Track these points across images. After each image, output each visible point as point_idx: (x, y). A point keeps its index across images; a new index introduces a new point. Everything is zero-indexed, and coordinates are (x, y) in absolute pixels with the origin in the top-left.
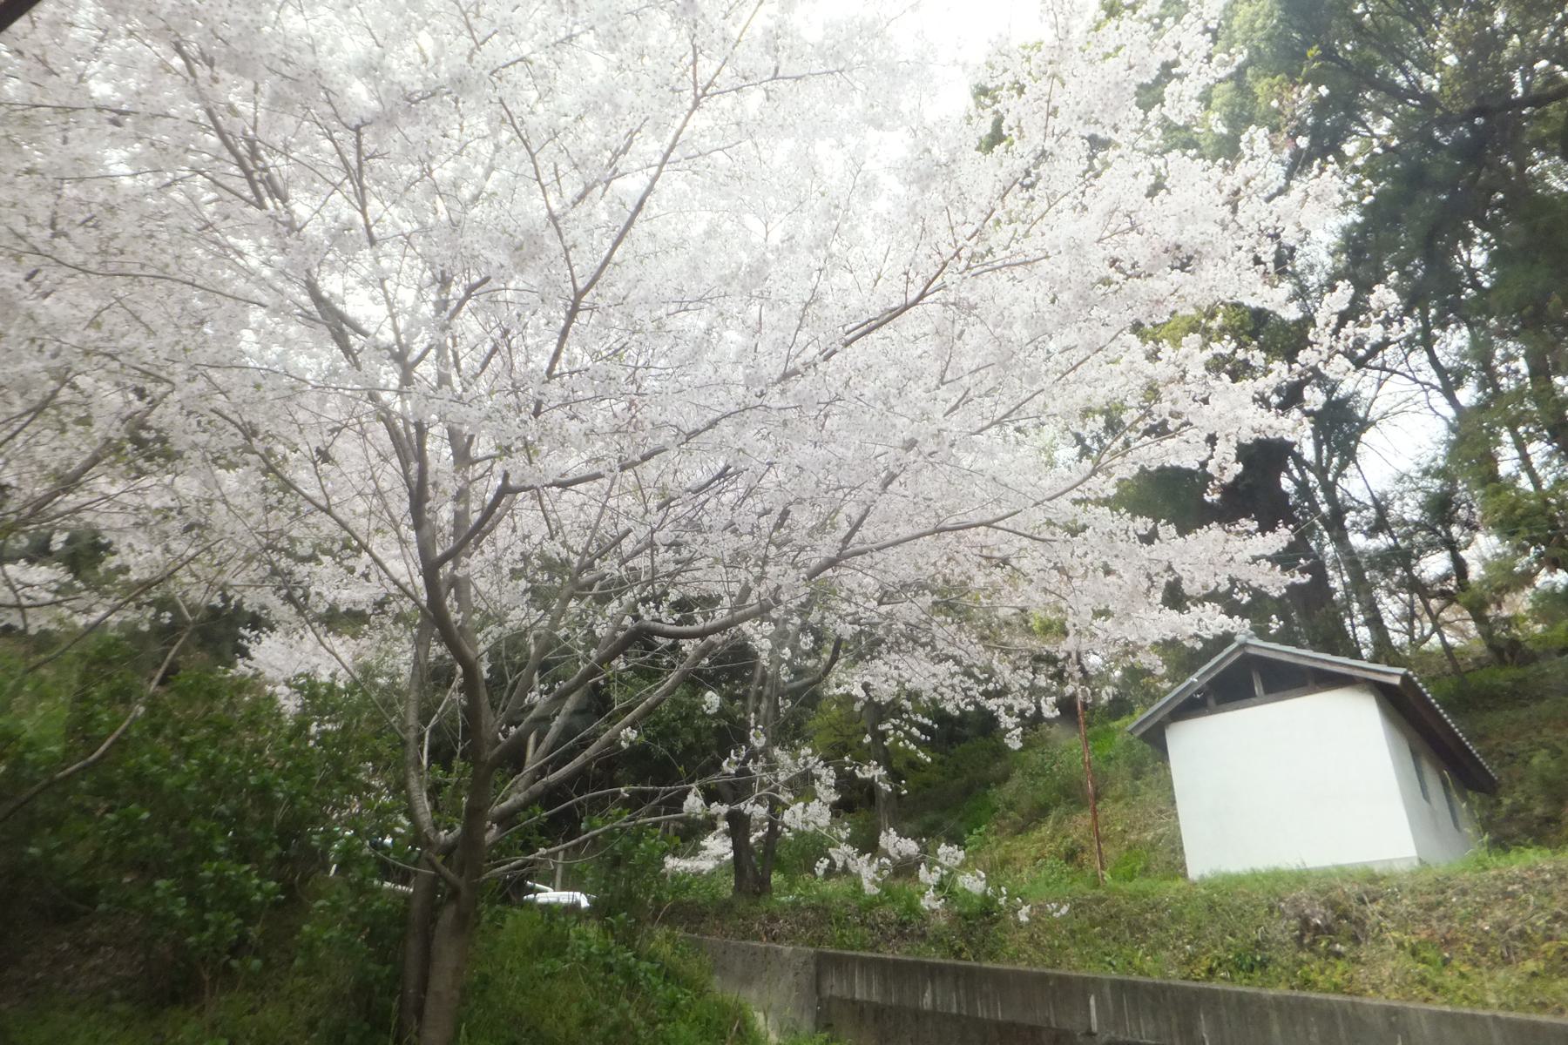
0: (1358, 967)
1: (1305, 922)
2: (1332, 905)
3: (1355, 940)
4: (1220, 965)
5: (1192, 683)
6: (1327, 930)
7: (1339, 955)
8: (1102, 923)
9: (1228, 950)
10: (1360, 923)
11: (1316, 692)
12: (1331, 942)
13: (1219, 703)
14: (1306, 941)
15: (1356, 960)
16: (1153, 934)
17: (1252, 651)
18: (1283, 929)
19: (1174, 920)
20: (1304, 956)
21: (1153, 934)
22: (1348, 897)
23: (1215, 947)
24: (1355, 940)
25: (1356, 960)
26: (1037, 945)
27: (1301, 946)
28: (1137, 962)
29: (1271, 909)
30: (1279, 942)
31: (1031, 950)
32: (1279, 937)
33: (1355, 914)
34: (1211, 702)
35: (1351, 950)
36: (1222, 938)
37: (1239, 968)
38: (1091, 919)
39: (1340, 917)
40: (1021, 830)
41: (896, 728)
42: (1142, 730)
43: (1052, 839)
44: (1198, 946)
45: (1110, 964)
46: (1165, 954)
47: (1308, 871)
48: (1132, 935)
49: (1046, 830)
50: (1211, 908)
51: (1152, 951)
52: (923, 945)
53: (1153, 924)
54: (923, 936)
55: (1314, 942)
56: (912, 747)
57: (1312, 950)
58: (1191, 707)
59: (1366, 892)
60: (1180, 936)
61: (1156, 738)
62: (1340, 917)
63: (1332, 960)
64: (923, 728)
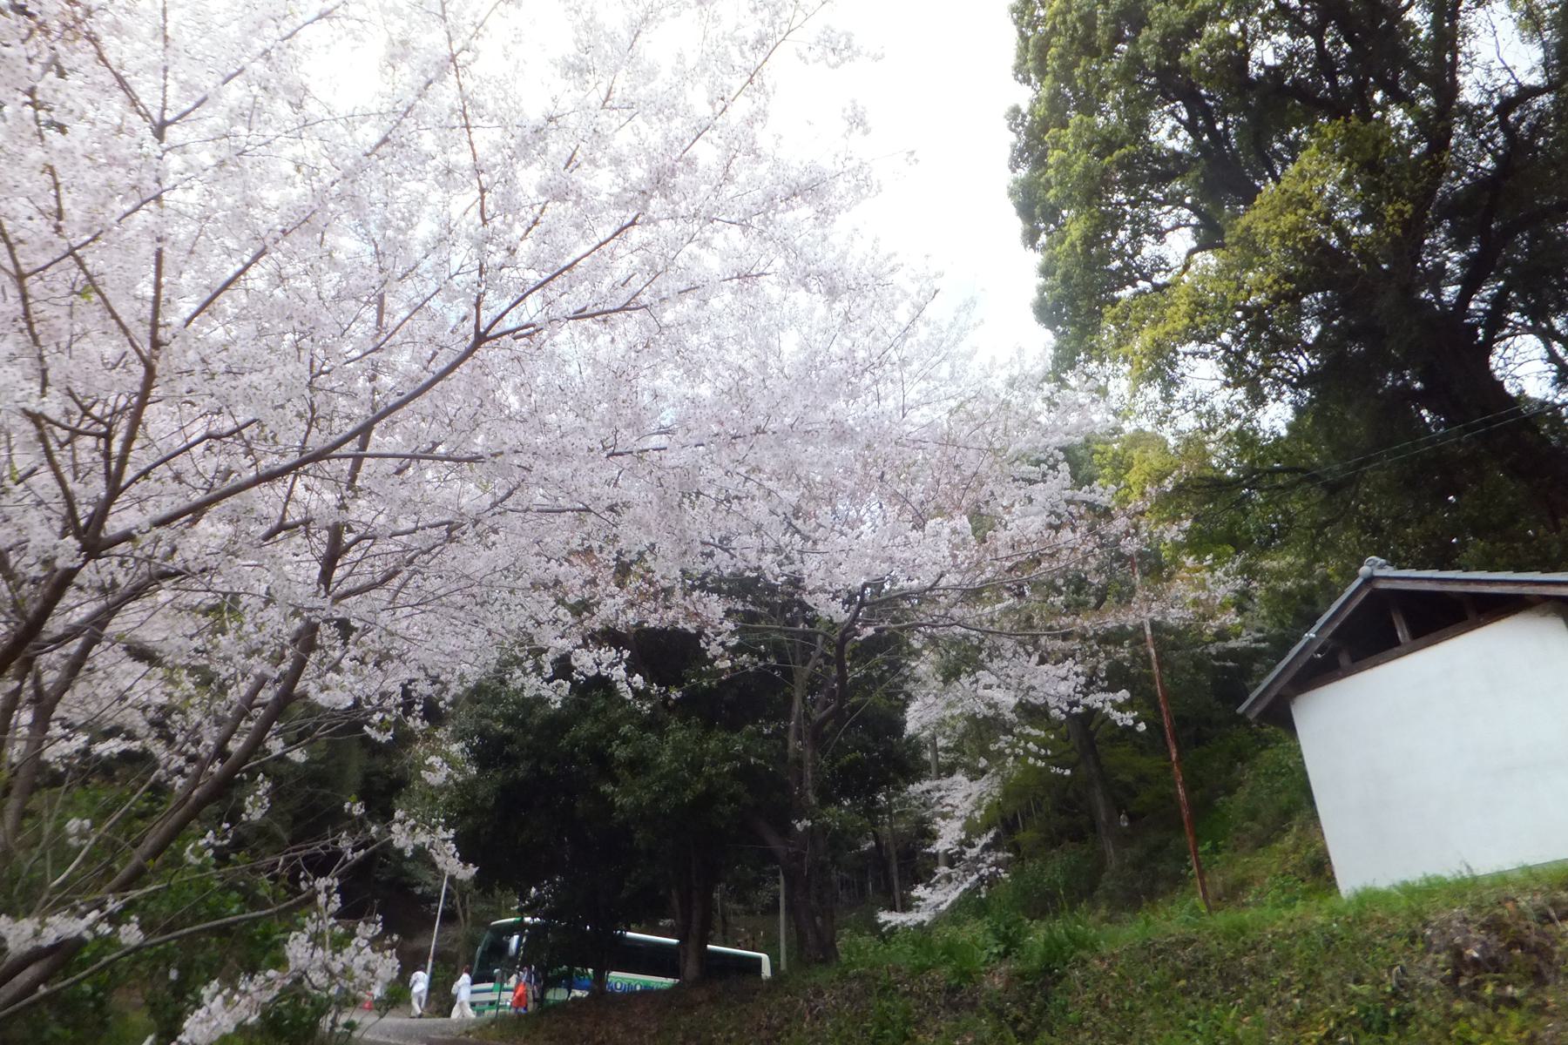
0: (1543, 1019)
1: (1458, 953)
2: (1494, 925)
3: (1538, 978)
4: (1340, 1025)
5: (1311, 640)
6: (1490, 965)
7: (1514, 1003)
8: (1189, 974)
9: (1349, 1003)
10: (1542, 952)
11: (1485, 624)
12: (1502, 984)
13: (1354, 660)
14: (1463, 983)
15: (1540, 1009)
16: (1253, 985)
17: (1382, 585)
18: (1430, 969)
19: (1278, 964)
20: (1459, 1007)
21: (1253, 985)
22: (1522, 915)
23: (1333, 998)
24: (1538, 978)
25: (1540, 1009)
26: (1105, 1011)
27: (1458, 994)
28: (1227, 1026)
29: (1413, 938)
30: (1424, 987)
31: (1096, 1015)
32: (1423, 979)
33: (1534, 938)
34: (1344, 660)
35: (1530, 994)
36: (1342, 986)
37: (1367, 1029)
38: (1175, 969)
39: (1511, 946)
40: (1263, 842)
41: (1013, 746)
42: (1258, 709)
43: (1296, 850)
44: (1313, 999)
45: (1194, 1029)
46: (1266, 1012)
47: (1475, 879)
48: (1226, 987)
49: (1289, 841)
50: (1329, 944)
51: (1250, 1009)
52: (973, 1017)
53: (1253, 971)
54: (973, 1005)
55: (1477, 985)
56: (1040, 764)
57: (1473, 998)
58: (1324, 669)
59: (1554, 904)
60: (1287, 984)
61: (1280, 717)
62: (1511, 946)
63: (1502, 1010)
64: (1042, 744)
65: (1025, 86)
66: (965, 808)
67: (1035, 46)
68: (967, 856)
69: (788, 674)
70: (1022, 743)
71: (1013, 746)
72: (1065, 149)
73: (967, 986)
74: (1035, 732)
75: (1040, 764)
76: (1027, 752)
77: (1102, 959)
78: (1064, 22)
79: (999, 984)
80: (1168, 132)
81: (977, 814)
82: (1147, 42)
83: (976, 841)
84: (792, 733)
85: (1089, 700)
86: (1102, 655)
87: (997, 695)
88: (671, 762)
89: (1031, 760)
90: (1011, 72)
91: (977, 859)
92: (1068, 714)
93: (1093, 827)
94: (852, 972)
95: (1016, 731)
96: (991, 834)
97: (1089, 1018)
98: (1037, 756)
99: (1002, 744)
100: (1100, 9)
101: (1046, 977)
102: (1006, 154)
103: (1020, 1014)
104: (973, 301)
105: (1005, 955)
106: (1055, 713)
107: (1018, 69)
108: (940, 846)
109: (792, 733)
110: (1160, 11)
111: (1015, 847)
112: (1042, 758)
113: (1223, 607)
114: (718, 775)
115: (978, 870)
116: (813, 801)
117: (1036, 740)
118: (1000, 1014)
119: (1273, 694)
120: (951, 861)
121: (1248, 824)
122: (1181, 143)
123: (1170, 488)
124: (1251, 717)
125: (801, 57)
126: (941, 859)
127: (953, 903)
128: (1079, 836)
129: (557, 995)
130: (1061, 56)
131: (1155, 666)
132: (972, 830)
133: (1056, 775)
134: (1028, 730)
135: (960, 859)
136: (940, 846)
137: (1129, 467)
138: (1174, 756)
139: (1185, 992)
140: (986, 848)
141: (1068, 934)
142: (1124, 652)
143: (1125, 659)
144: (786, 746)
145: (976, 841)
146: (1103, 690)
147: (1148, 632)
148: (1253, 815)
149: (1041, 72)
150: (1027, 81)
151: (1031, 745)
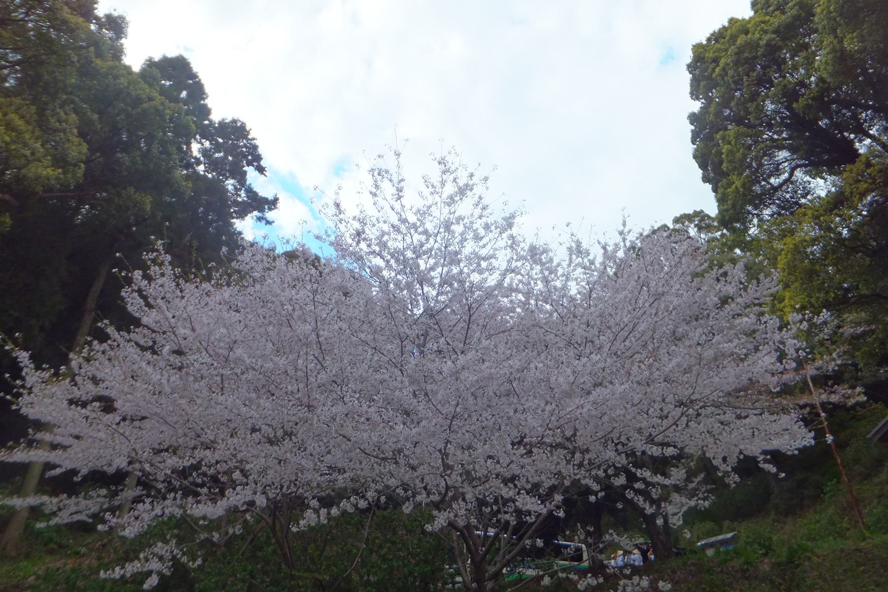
26: (825, 580)
42: (878, 436)
65: (697, 102)
72: (730, 143)
73: (751, 569)
77: (818, 557)
79: (767, 567)
83: (694, 480)
90: (689, 96)
91: (695, 489)
94: (689, 562)
97: (817, 584)
101: (792, 562)
102: (689, 135)
103: (781, 581)
105: (766, 555)
107: (692, 94)
115: (697, 495)
118: (772, 581)
119: (885, 429)
127: (685, 512)
129: (576, 578)
137: (782, 300)
139: (864, 572)
141: (799, 546)
145: (694, 480)
150: (697, 98)
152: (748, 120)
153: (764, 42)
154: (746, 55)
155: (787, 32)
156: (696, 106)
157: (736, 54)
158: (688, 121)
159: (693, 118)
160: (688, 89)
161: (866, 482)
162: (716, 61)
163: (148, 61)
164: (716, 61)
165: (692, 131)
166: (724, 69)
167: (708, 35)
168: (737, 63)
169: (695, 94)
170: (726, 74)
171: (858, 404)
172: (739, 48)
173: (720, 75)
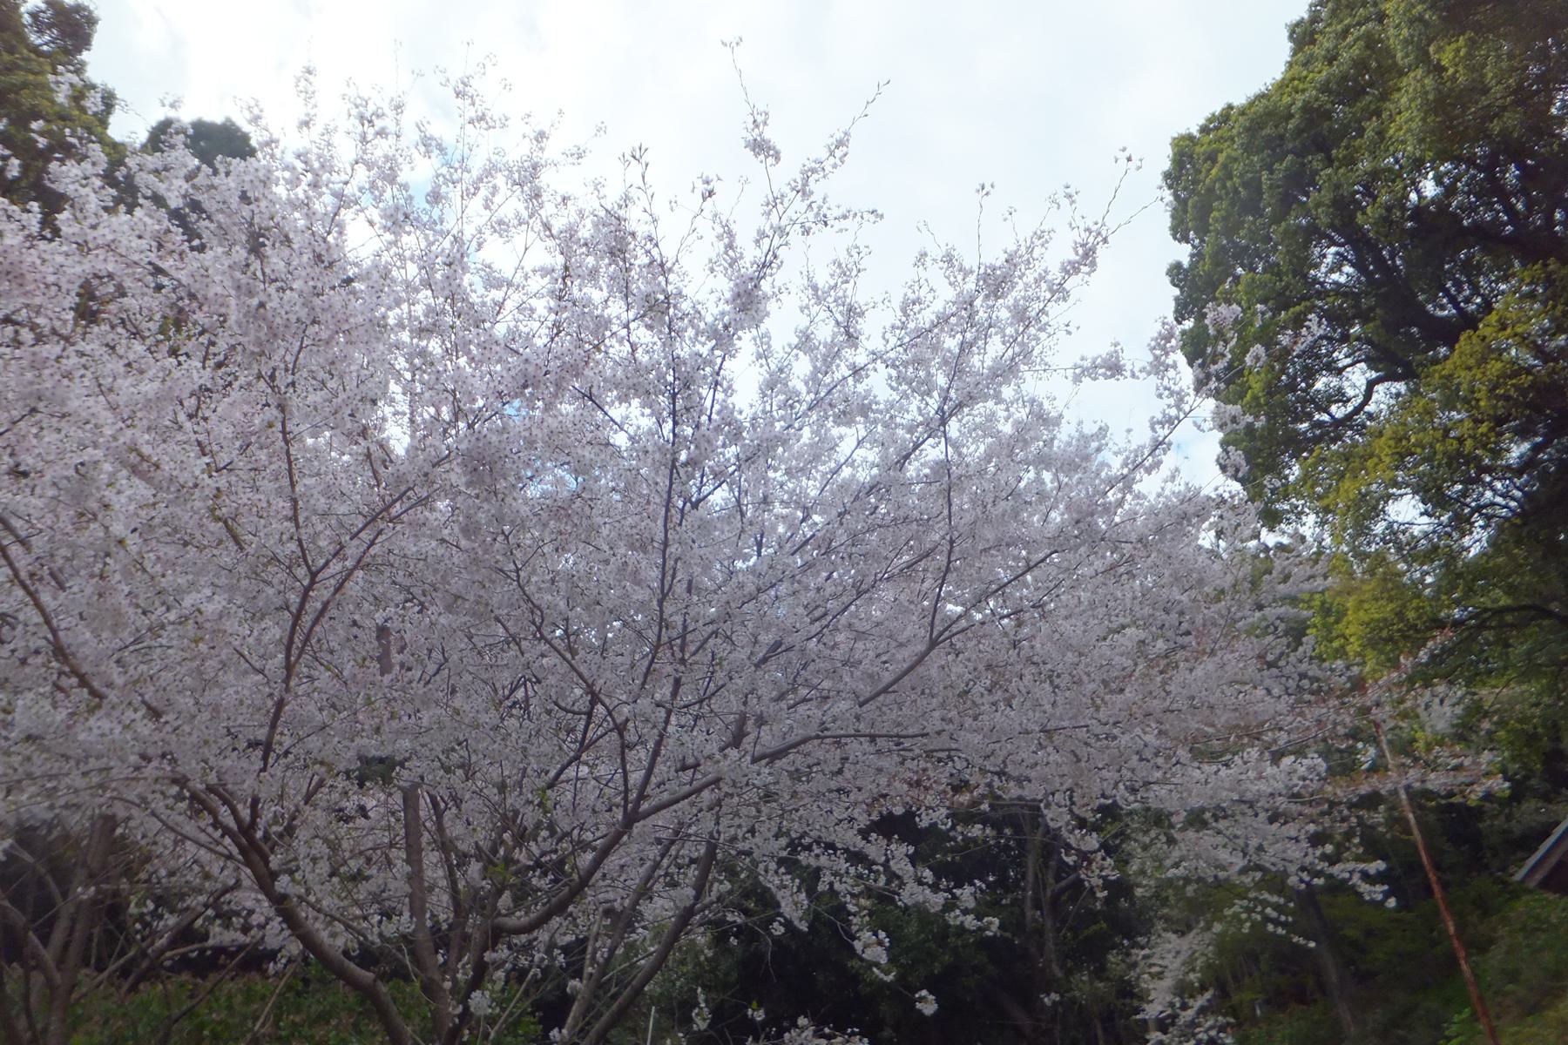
42: (1539, 876)
56: (1280, 931)
65: (1184, 245)
66: (1174, 965)
67: (1194, 207)
68: (1181, 1021)
69: (1021, 844)
70: (1259, 909)
71: (1249, 910)
74: (1275, 899)
75: (1280, 931)
76: (1267, 919)
78: (1224, 186)
80: (1334, 268)
81: (1192, 976)
82: (1318, 205)
83: (1191, 1002)
84: (1029, 903)
85: (1336, 869)
86: (1354, 820)
87: (1224, 855)
88: (918, 933)
89: (1270, 927)
91: (1193, 1024)
92: (1308, 884)
93: (1322, 987)
95: (1252, 895)
96: (1208, 995)
98: (1276, 923)
99: (1236, 909)
100: (1265, 175)
104: (1177, 470)
106: (1293, 880)
108: (1152, 1011)
109: (1029, 903)
110: (1329, 176)
111: (1234, 1011)
112: (1284, 925)
113: (1488, 774)
114: (964, 946)
115: (1194, 1035)
116: (1059, 974)
117: (1276, 907)
119: (1554, 860)
120: (1163, 1026)
121: (1510, 987)
122: (1344, 275)
123: (1425, 659)
124: (1532, 884)
125: (1199, 427)
126: (1151, 1025)
128: (1302, 997)
130: (1225, 219)
131: (1416, 832)
132: (1184, 990)
133: (1296, 945)
134: (1266, 896)
135: (1173, 1024)
136: (1152, 1011)
137: (1341, 615)
138: (1452, 929)
140: (1202, 1011)
142: (1378, 817)
143: (1379, 824)
144: (1023, 914)
145: (1191, 1002)
146: (1358, 859)
147: (1404, 796)
148: (1513, 976)
149: (1202, 231)
150: (1185, 239)
151: (1269, 910)
152: (1292, 294)
153: (1299, 104)
154: (1267, 131)
155: (1348, 89)
156: (1183, 253)
157: (1248, 130)
158: (1168, 279)
159: (1175, 272)
160: (1166, 220)
161: (1530, 1019)
162: (1212, 158)
163: (1003, 844)
164: (1212, 158)
165: (1177, 299)
166: (1225, 166)
167: (1202, 122)
168: (1248, 149)
169: (1179, 231)
170: (1230, 177)
171: (1489, 796)
172: (1252, 120)
173: (1219, 179)
